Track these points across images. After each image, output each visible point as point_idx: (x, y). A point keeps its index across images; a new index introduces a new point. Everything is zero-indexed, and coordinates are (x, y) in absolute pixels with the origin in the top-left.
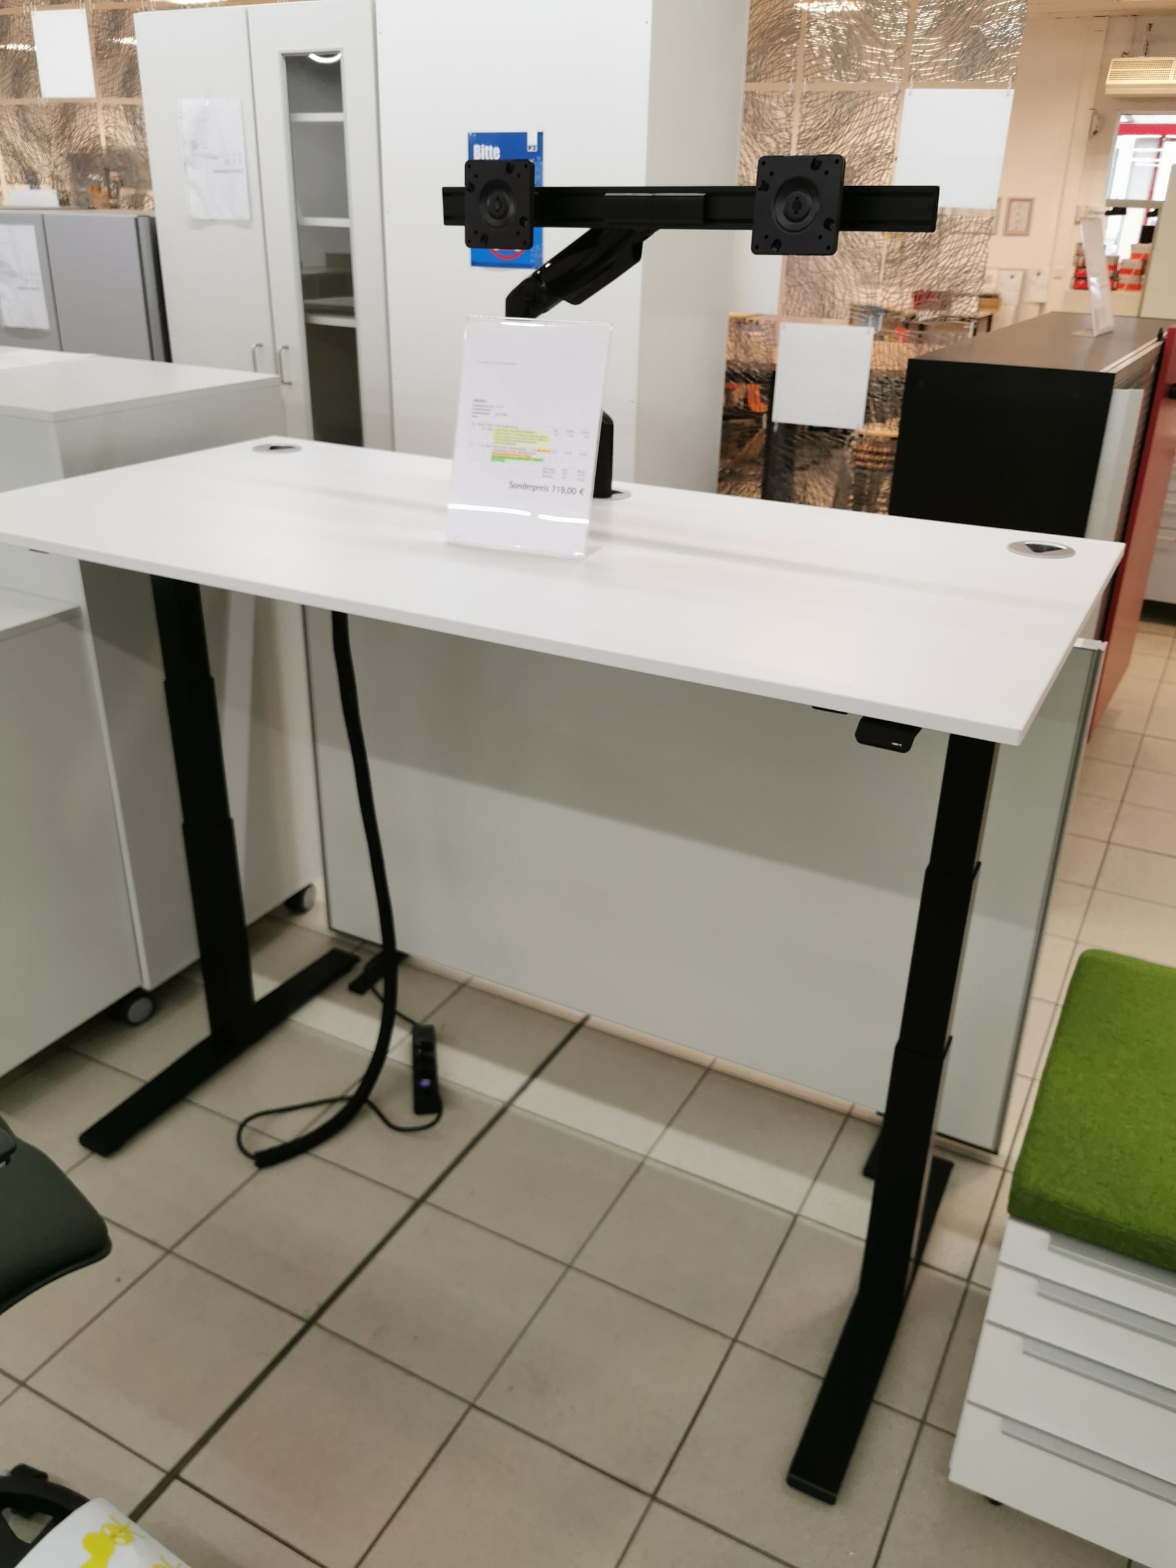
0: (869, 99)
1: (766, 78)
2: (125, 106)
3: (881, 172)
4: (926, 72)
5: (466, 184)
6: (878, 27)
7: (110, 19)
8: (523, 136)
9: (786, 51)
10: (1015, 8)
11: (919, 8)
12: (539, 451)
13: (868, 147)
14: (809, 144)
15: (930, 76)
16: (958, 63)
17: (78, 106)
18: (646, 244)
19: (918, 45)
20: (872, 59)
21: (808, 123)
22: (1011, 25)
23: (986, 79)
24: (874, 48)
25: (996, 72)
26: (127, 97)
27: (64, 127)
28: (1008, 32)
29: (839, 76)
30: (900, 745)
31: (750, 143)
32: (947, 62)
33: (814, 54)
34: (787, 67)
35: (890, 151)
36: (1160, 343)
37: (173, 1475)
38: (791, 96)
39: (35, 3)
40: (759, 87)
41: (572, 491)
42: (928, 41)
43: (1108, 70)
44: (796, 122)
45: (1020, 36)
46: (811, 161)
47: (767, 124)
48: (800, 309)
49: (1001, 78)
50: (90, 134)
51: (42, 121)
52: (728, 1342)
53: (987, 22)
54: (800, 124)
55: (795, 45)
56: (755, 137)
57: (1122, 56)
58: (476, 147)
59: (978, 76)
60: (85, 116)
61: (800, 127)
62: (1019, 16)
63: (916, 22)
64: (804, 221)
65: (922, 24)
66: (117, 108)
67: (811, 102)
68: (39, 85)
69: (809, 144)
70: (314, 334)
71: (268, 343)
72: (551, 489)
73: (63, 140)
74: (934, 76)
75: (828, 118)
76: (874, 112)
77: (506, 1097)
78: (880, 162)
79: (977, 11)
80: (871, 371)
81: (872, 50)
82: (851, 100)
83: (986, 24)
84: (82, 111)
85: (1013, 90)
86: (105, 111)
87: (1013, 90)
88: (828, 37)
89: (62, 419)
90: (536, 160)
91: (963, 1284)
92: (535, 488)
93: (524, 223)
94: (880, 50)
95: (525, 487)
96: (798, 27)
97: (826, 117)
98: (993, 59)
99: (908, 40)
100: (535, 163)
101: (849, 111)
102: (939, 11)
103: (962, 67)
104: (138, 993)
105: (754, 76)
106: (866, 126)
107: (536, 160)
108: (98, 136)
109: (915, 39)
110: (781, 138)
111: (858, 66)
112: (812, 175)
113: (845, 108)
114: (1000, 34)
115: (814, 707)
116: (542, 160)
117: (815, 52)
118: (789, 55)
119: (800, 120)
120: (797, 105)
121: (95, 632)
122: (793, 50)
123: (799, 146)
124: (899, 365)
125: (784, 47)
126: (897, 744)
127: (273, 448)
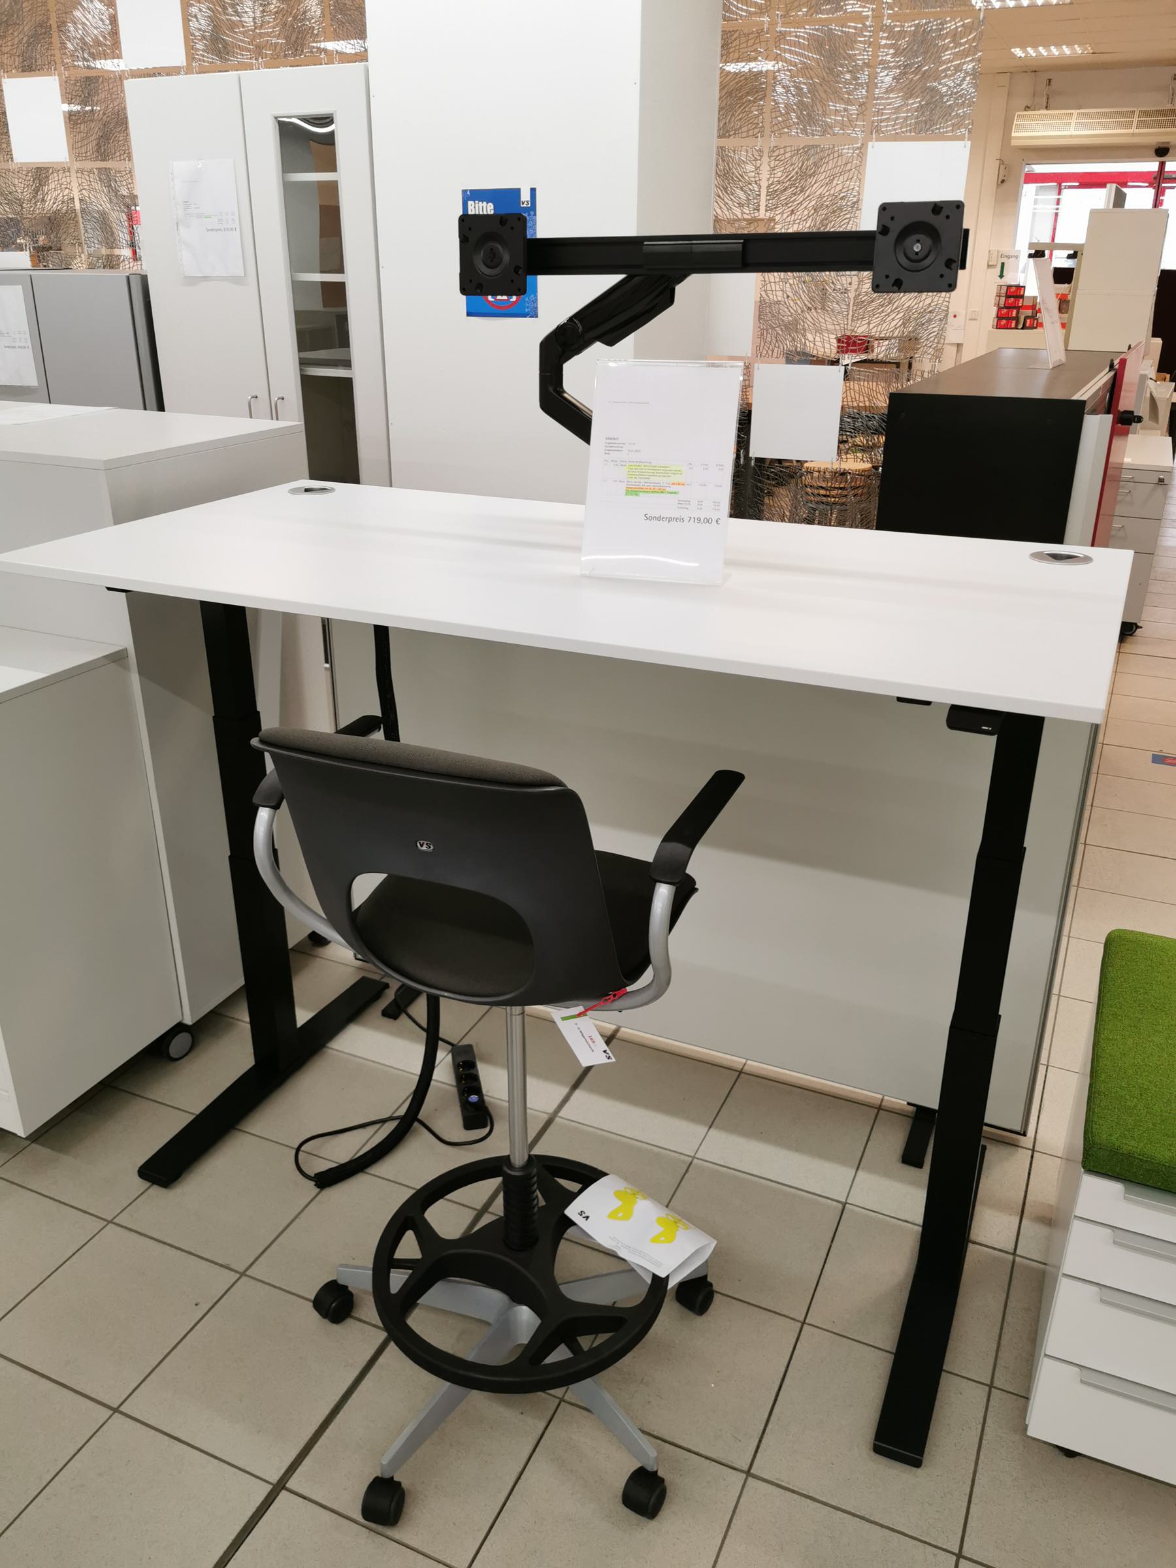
0: (834, 152)
1: (735, 134)
2: (99, 169)
3: (847, 220)
4: (887, 126)
5: (878, 228)
6: (840, 85)
7: (84, 87)
8: (516, 192)
9: (753, 109)
10: (969, 67)
11: (879, 68)
12: (673, 484)
13: (834, 197)
14: (778, 195)
15: (890, 131)
16: (917, 118)
17: (51, 171)
18: (679, 288)
19: (879, 102)
20: (836, 115)
21: (776, 176)
22: (966, 83)
23: (944, 132)
24: (838, 105)
25: (953, 125)
26: (102, 160)
27: (36, 191)
28: (962, 89)
29: (804, 131)
30: (990, 729)
31: (721, 195)
32: (908, 116)
33: (780, 111)
34: (754, 124)
35: (855, 199)
36: (1112, 373)
37: (280, 1486)
38: (760, 150)
39: (6, 71)
40: (729, 143)
41: (708, 521)
42: (888, 98)
43: (1013, 123)
44: (765, 175)
45: (974, 92)
46: (932, 206)
47: (737, 177)
48: (773, 351)
49: (958, 131)
50: (63, 196)
51: (14, 185)
52: (799, 1325)
53: (943, 79)
54: (768, 176)
55: (762, 103)
56: (726, 189)
57: (1025, 110)
58: (470, 203)
59: (937, 129)
60: (59, 180)
61: (768, 179)
62: (972, 74)
63: (876, 81)
64: (925, 261)
65: (883, 82)
66: (91, 171)
67: (779, 155)
68: (11, 151)
69: (778, 195)
70: (309, 385)
71: (263, 395)
72: (686, 519)
73: (35, 204)
74: (895, 130)
75: (795, 171)
76: (839, 164)
77: (551, 1110)
78: (845, 211)
79: (934, 69)
80: (843, 408)
81: (835, 106)
82: (817, 153)
83: (942, 81)
84: (55, 175)
85: (970, 142)
86: (79, 175)
87: (970, 142)
88: (793, 96)
89: (112, 467)
90: (529, 215)
91: (1011, 1257)
92: (670, 520)
93: (518, 271)
94: (843, 106)
95: (660, 518)
96: (764, 86)
97: (793, 170)
98: (950, 114)
99: (870, 95)
100: (528, 218)
101: (815, 164)
102: (898, 71)
103: (922, 121)
104: (180, 1028)
105: (724, 133)
106: (832, 178)
107: (529, 215)
108: (72, 199)
109: (876, 96)
110: (751, 190)
111: (823, 121)
112: (936, 221)
113: (812, 160)
114: (955, 90)
115: (900, 699)
116: (535, 215)
117: (781, 109)
118: (756, 113)
119: (769, 173)
120: (765, 159)
121: (140, 673)
122: (760, 108)
123: (768, 198)
124: (869, 400)
125: (751, 105)
126: (987, 728)
127: (307, 490)
